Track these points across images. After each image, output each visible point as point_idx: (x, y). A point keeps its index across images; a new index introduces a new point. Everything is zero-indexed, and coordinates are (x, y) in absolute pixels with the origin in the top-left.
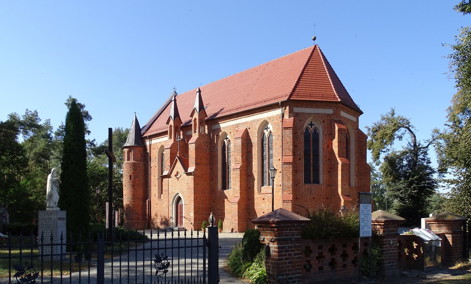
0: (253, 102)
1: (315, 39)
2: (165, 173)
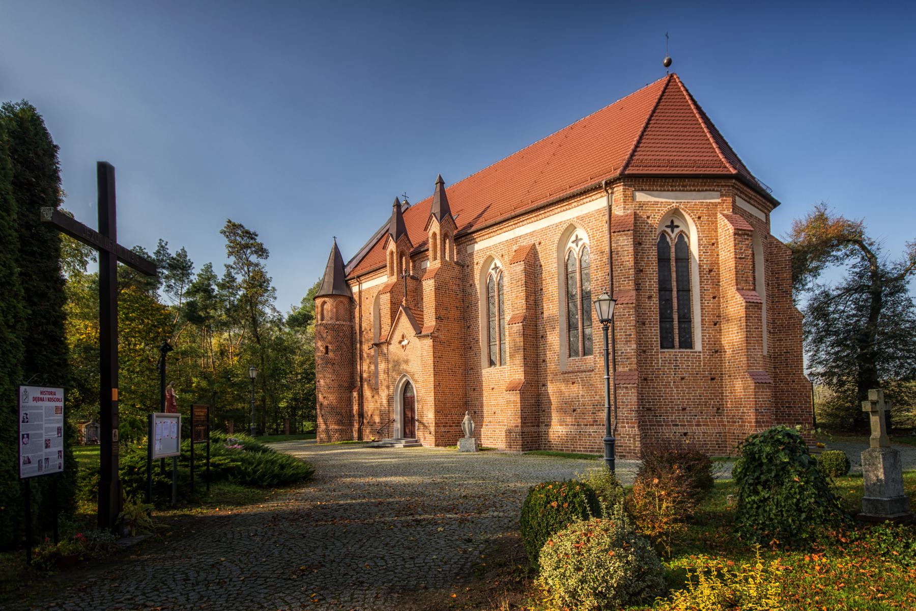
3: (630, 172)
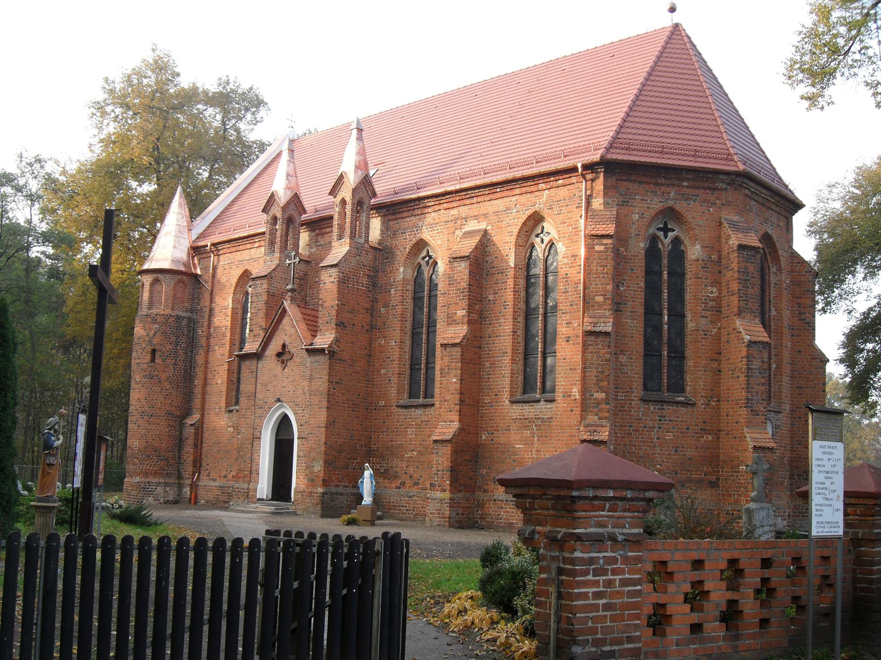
0: (505, 161)
1: (672, 10)
2: (251, 347)
3: (614, 157)
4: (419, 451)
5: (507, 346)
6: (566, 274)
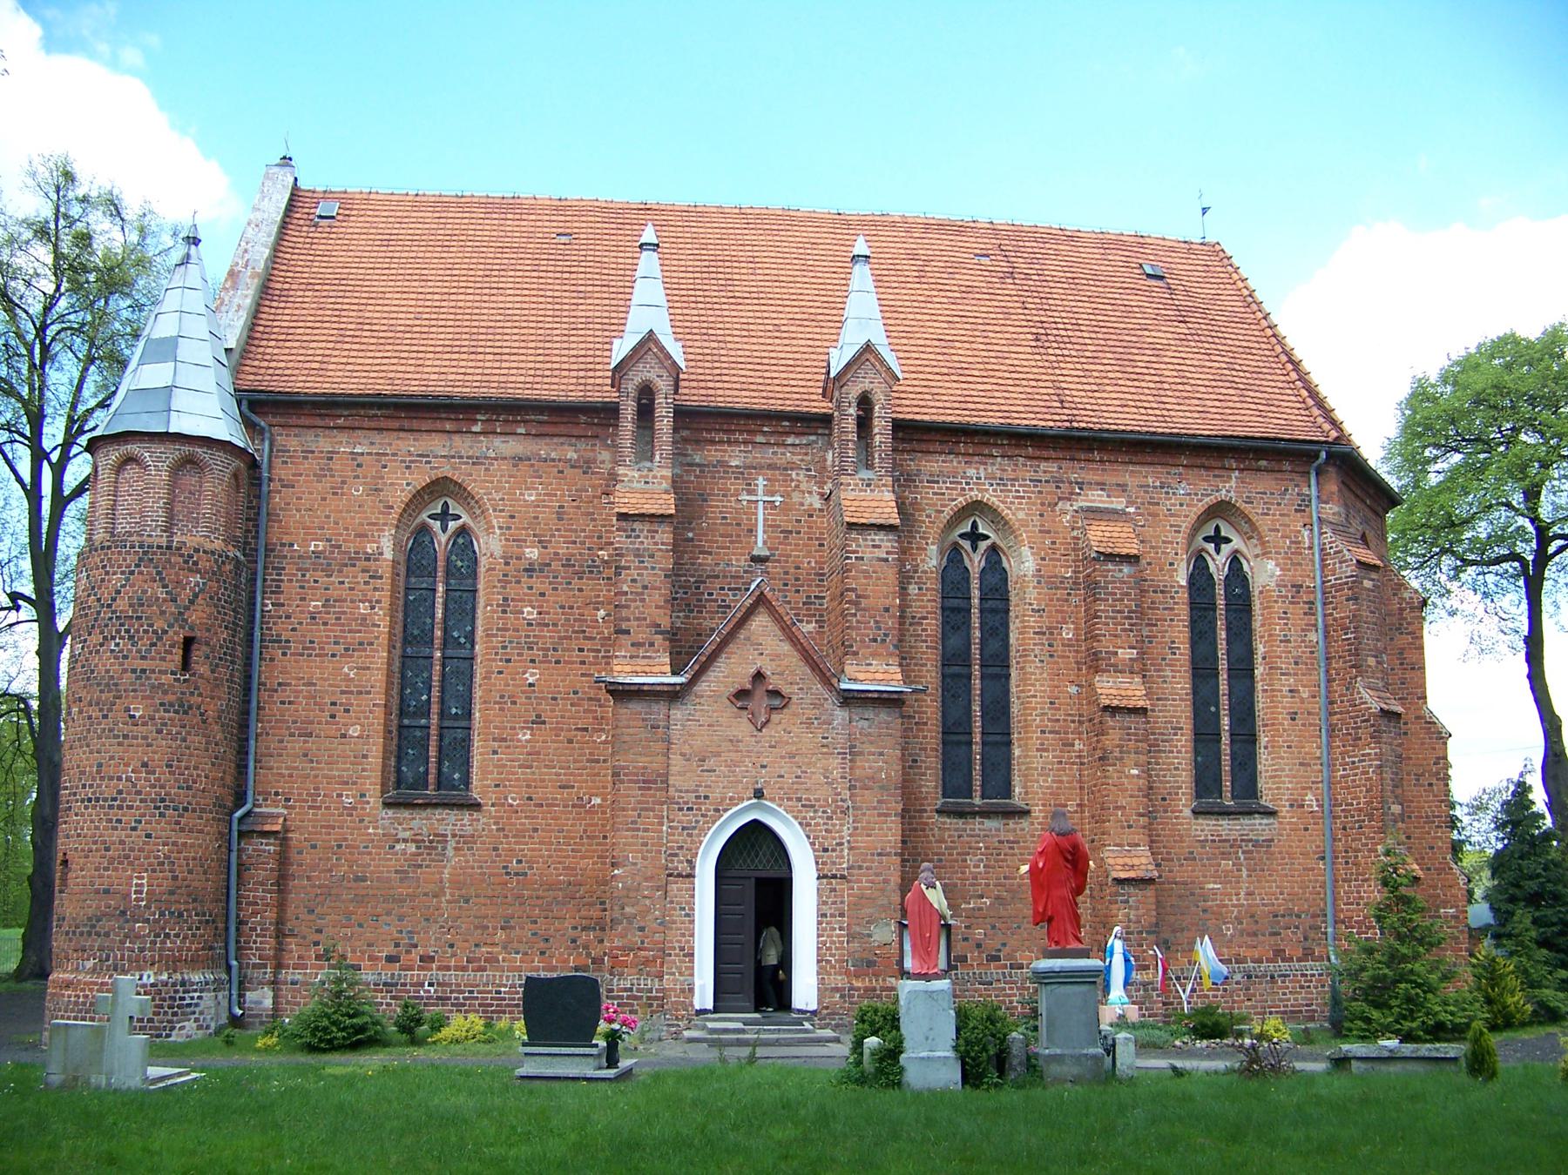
4: (998, 898)
5: (1181, 717)
6: (1285, 613)
